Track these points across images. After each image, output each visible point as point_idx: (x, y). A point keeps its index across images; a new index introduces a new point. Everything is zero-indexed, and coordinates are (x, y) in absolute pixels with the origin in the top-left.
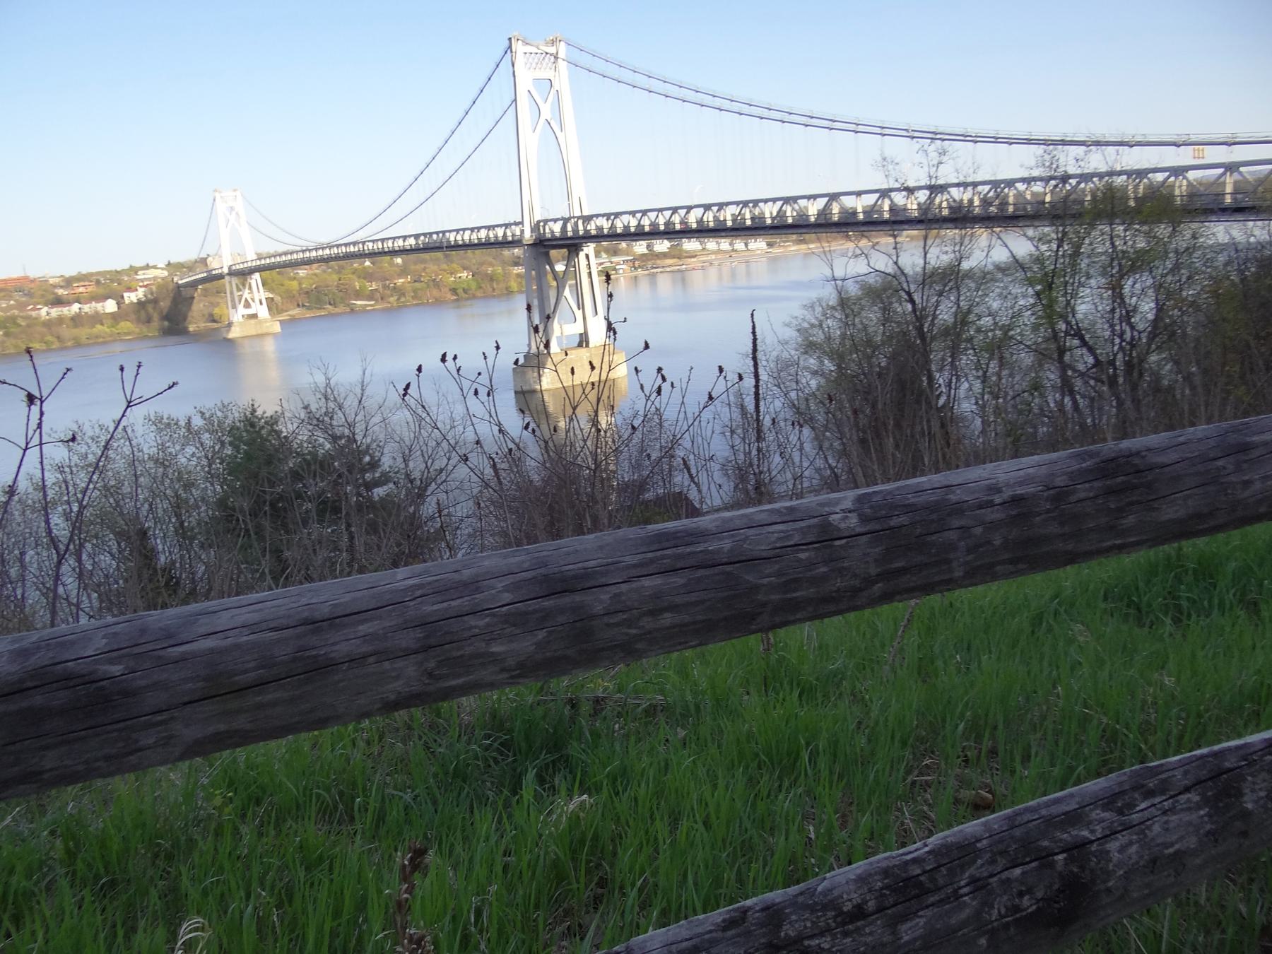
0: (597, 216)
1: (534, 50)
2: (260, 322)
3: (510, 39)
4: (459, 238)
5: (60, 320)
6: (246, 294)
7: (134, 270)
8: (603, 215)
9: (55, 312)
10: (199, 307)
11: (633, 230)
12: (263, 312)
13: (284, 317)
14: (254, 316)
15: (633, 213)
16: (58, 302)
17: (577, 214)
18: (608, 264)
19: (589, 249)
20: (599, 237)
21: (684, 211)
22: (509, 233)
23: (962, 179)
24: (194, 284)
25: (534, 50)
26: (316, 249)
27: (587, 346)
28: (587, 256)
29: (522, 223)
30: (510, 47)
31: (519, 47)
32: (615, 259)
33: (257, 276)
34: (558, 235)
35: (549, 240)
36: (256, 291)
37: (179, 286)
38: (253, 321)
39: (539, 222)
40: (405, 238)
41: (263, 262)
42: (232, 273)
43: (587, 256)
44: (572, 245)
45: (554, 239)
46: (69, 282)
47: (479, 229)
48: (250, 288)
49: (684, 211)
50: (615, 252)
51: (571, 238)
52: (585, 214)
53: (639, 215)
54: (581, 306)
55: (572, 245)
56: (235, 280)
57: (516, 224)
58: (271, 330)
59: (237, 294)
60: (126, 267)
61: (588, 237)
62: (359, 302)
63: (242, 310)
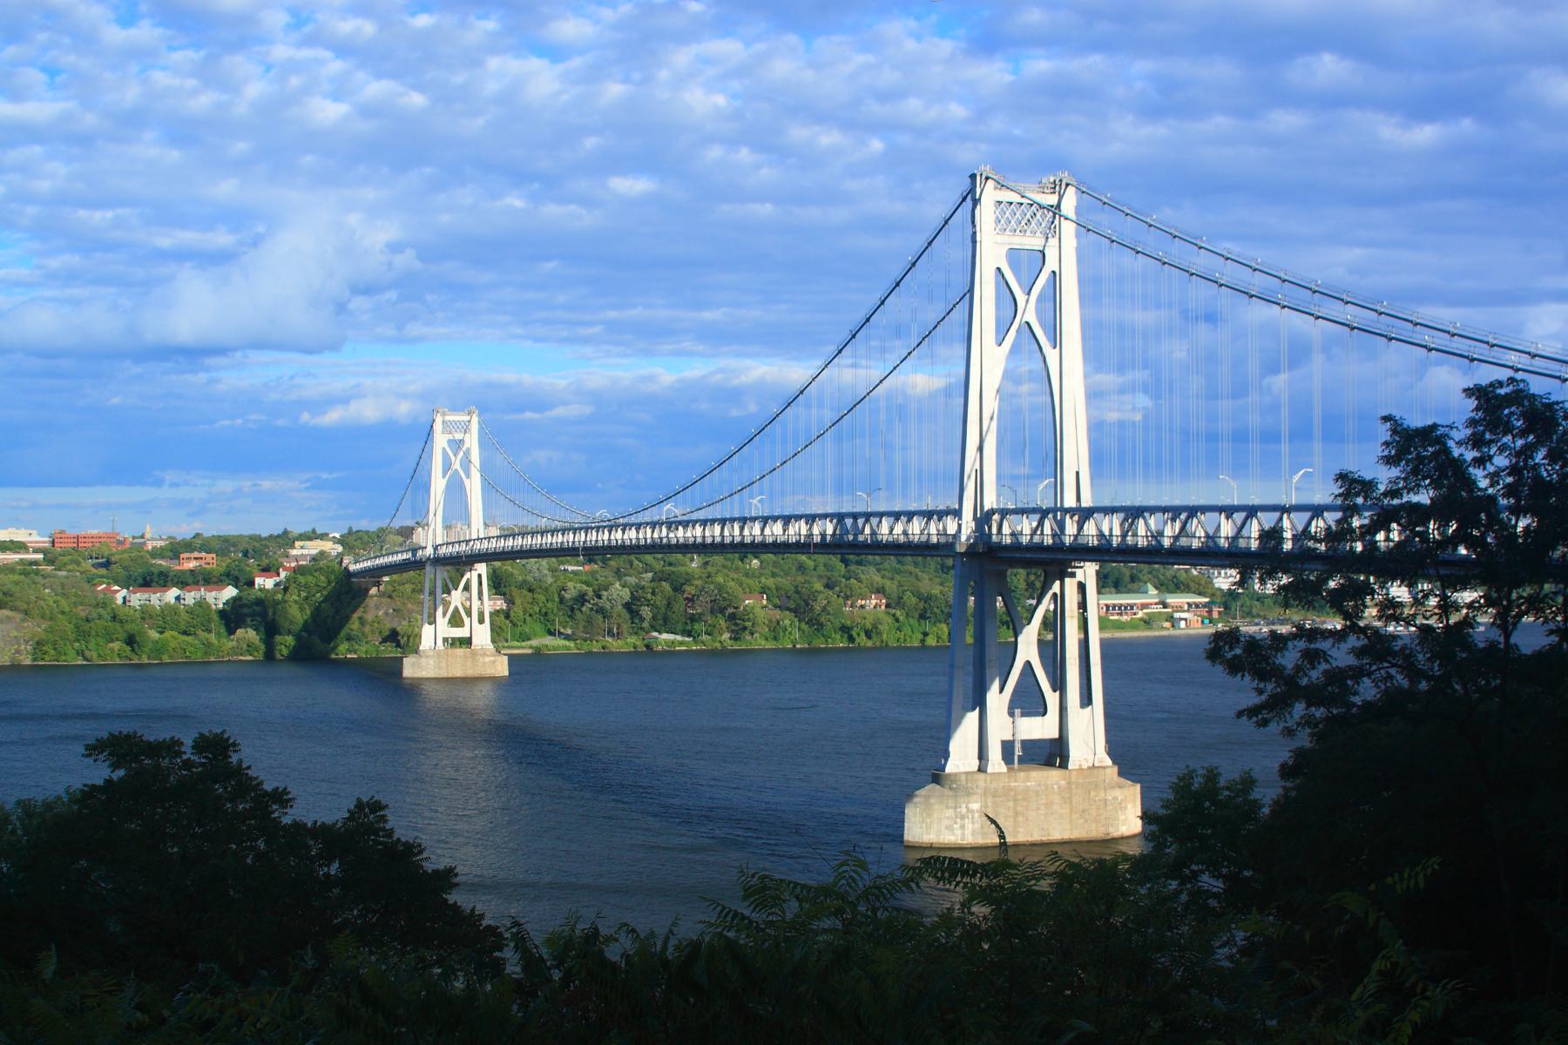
0: (1153, 510)
1: (1016, 198)
2: (474, 654)
3: (973, 177)
4: (899, 529)
5: (146, 613)
6: (457, 598)
7: (286, 540)
8: (1164, 510)
9: (137, 599)
10: (375, 610)
11: (1166, 543)
12: (482, 636)
13: (524, 649)
14: (467, 642)
15: (1229, 511)
16: (148, 581)
17: (1070, 502)
19: (1088, 572)
20: (1101, 552)
21: (1243, 515)
22: (816, 531)
23: (1020, 505)
24: (376, 573)
25: (1016, 198)
27: (1064, 765)
28: (1082, 588)
29: (957, 513)
30: (972, 190)
31: (990, 195)
32: (1172, 600)
33: (481, 568)
34: (1223, 543)
36: (474, 597)
37: (348, 574)
38: (460, 651)
39: (992, 512)
40: (811, 519)
42: (438, 561)
43: (1082, 588)
44: (1053, 561)
45: (1016, 547)
46: (176, 549)
47: (910, 515)
48: (467, 588)
49: (1243, 515)
50: (1178, 586)
51: (1048, 549)
52: (1084, 505)
53: (1239, 517)
54: (1059, 684)
55: (1053, 561)
56: (442, 574)
57: (947, 512)
59: (440, 595)
60: (278, 531)
61: (1082, 552)
62: (665, 636)
63: (443, 628)
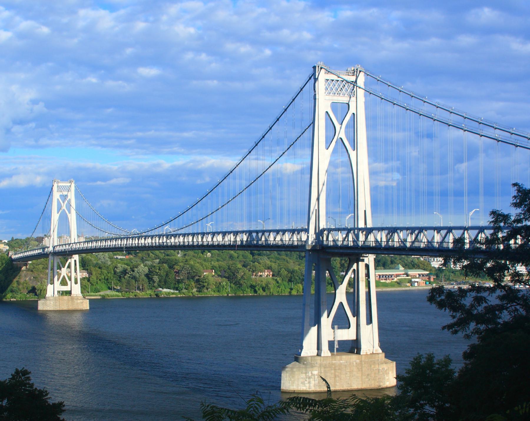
1: (335, 78)
2: (73, 299)
3: (314, 67)
4: (278, 238)
6: (64, 271)
8: (407, 229)
11: (408, 245)
12: (76, 290)
14: (69, 293)
15: (438, 229)
17: (361, 225)
18: (405, 277)
19: (370, 259)
21: (445, 231)
22: (238, 239)
25: (335, 78)
26: (127, 238)
27: (358, 352)
28: (367, 266)
29: (307, 231)
30: (314, 74)
31: (322, 76)
32: (411, 272)
33: (76, 257)
34: (436, 245)
35: (331, 247)
36: (73, 271)
38: (66, 298)
41: (90, 245)
42: (56, 254)
43: (367, 266)
44: (353, 254)
45: (335, 247)
47: (284, 232)
48: (69, 267)
53: (443, 232)
55: (353, 254)
56: (58, 260)
58: (80, 307)
62: (165, 290)
63: (58, 286)
